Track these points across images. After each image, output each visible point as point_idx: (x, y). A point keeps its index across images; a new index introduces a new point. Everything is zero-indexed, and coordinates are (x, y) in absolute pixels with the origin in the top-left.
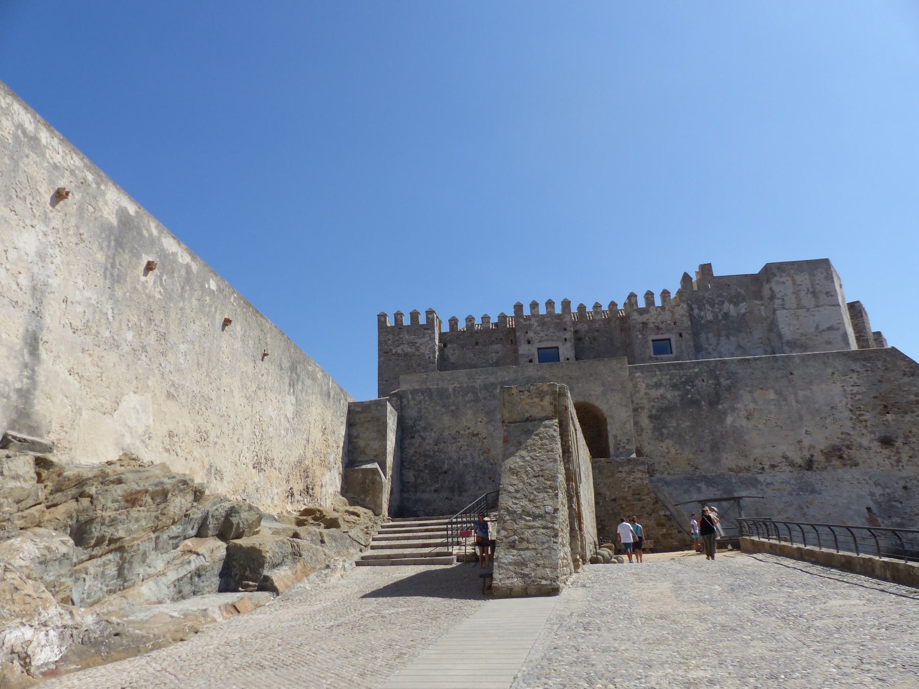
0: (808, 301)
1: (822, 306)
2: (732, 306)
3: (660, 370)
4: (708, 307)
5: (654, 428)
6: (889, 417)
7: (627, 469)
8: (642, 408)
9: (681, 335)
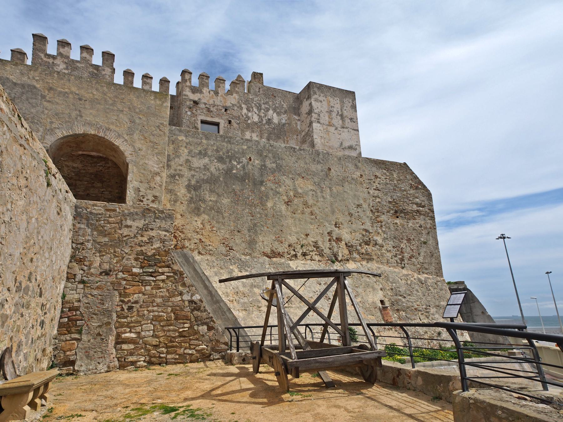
0: (337, 121)
1: (347, 128)
2: (275, 115)
3: (207, 138)
4: (255, 110)
5: (191, 201)
6: (398, 221)
7: (140, 223)
8: (181, 176)
9: (230, 122)
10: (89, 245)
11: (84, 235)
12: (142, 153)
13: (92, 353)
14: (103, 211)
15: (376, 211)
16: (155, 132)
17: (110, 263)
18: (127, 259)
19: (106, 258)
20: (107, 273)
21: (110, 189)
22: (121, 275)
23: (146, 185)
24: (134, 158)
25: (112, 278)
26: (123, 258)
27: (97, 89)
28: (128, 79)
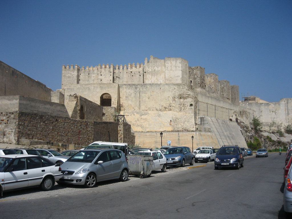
0: (174, 68)
15: (174, 98)
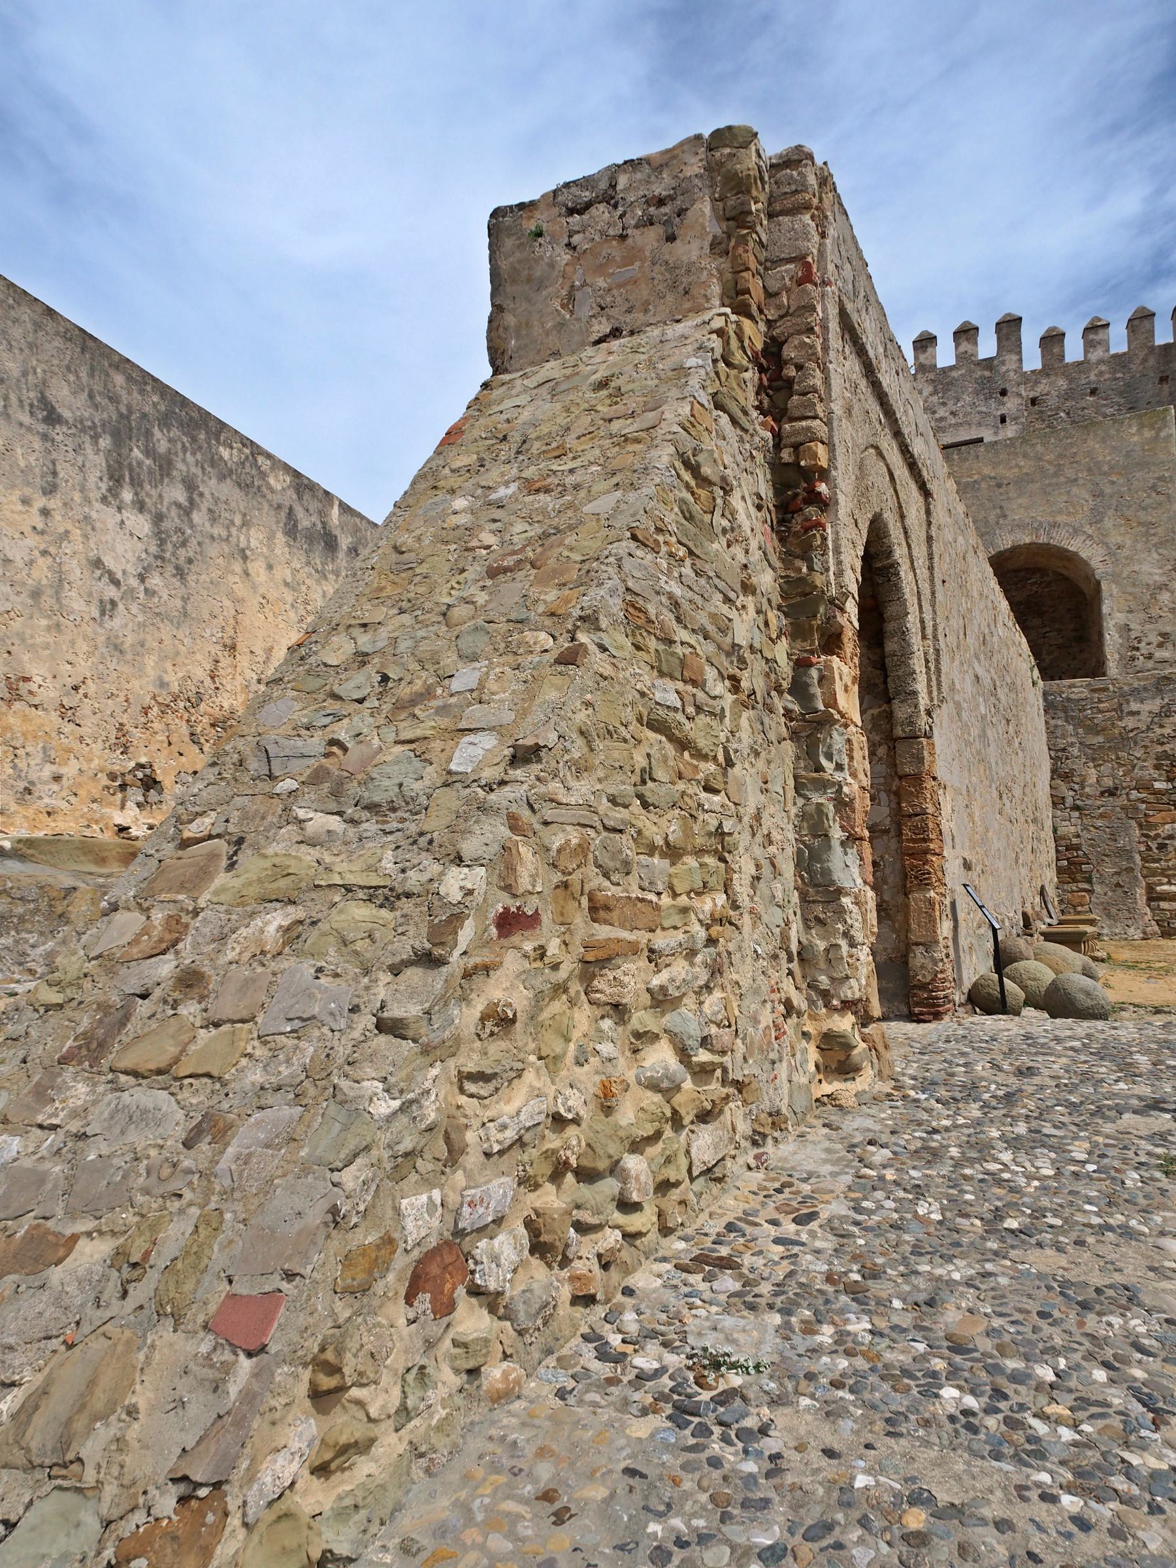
7: (1154, 705)
10: (1076, 752)
11: (1064, 737)
12: (1125, 552)
13: (1113, 911)
14: (1086, 693)
16: (1148, 501)
17: (1114, 777)
18: (1141, 768)
19: (1106, 768)
20: (1112, 792)
21: (1057, 626)
22: (1134, 794)
23: (1142, 615)
24: (1110, 568)
25: (1123, 801)
26: (1134, 767)
27: (1025, 456)
28: (1052, 354)
